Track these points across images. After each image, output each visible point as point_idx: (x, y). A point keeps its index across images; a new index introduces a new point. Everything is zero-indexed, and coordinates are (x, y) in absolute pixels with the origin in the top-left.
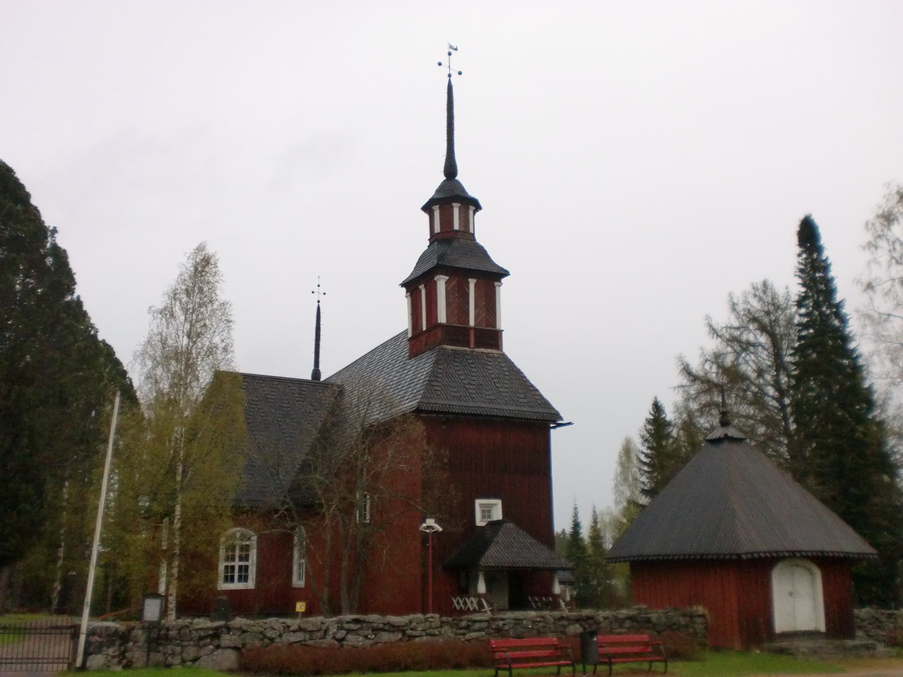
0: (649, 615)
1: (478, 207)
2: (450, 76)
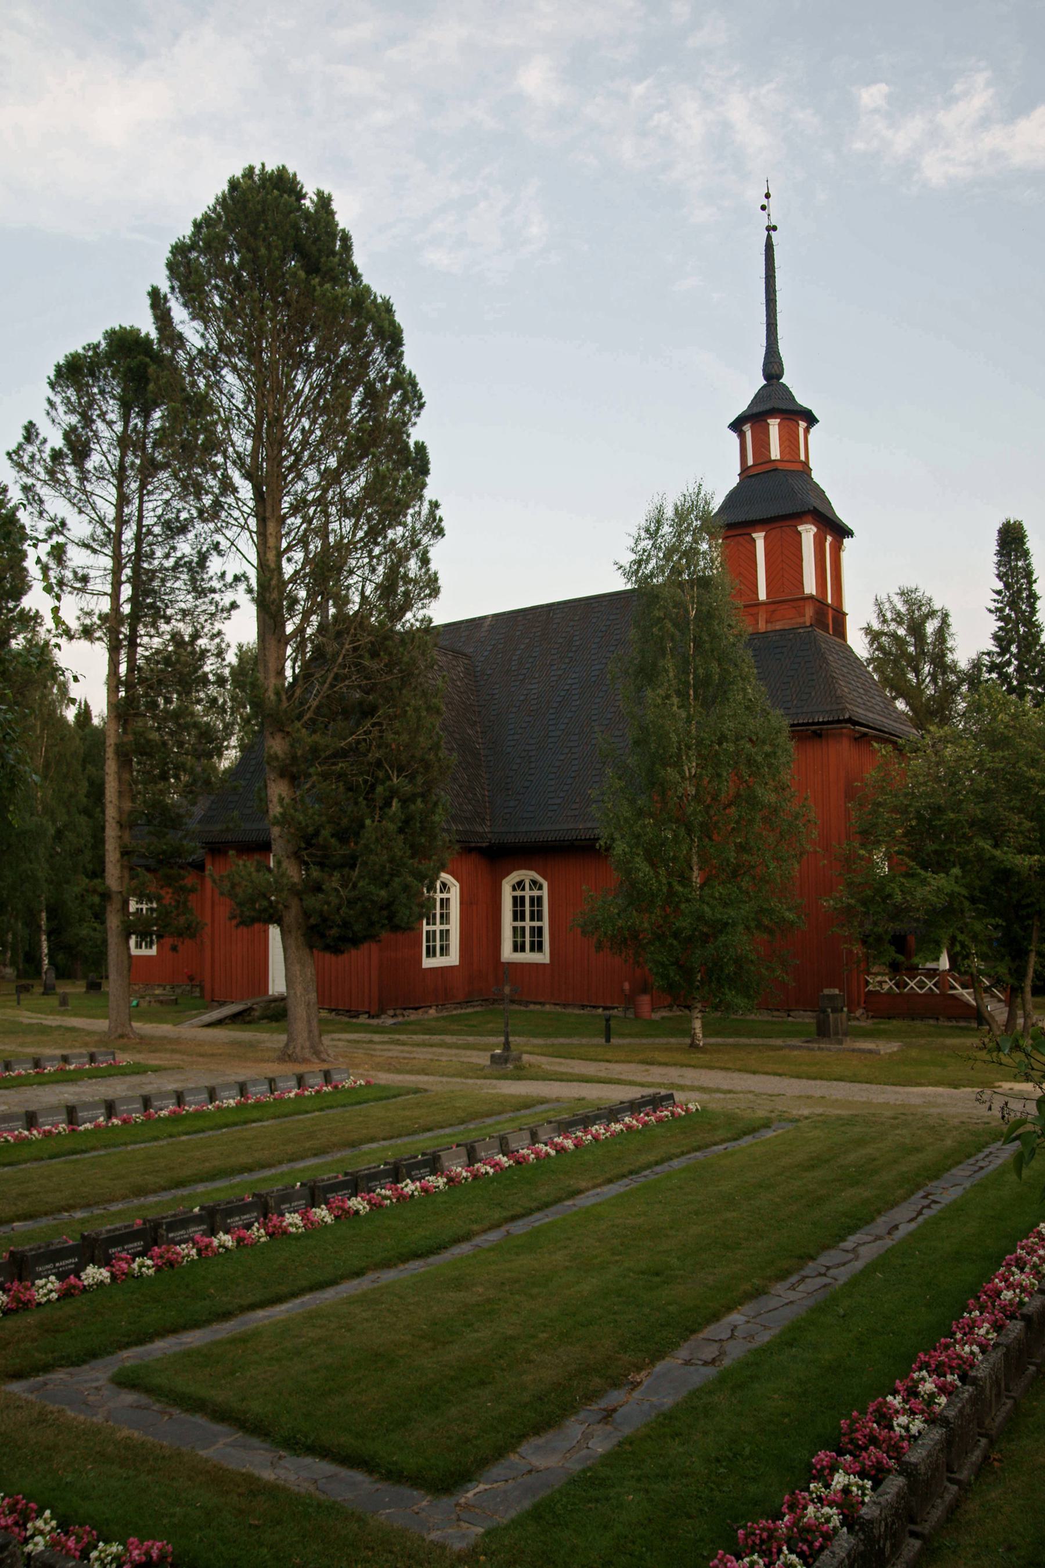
1: (811, 419)
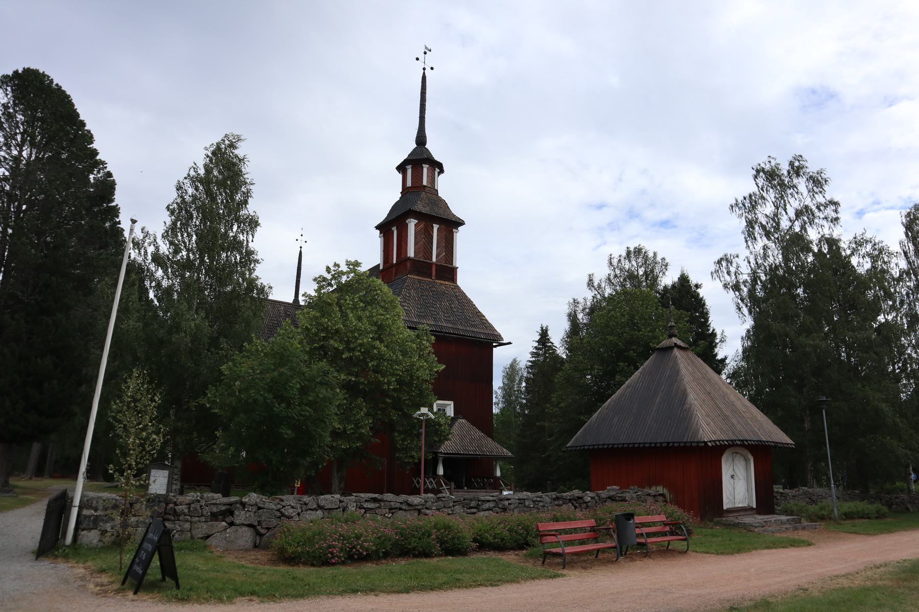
0: (624, 495)
2: (424, 69)
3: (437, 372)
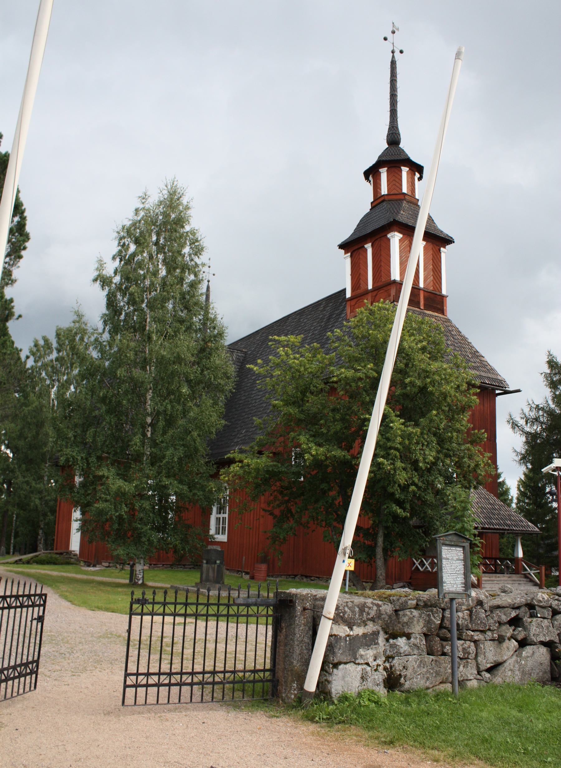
2: (393, 52)
3: (417, 425)
